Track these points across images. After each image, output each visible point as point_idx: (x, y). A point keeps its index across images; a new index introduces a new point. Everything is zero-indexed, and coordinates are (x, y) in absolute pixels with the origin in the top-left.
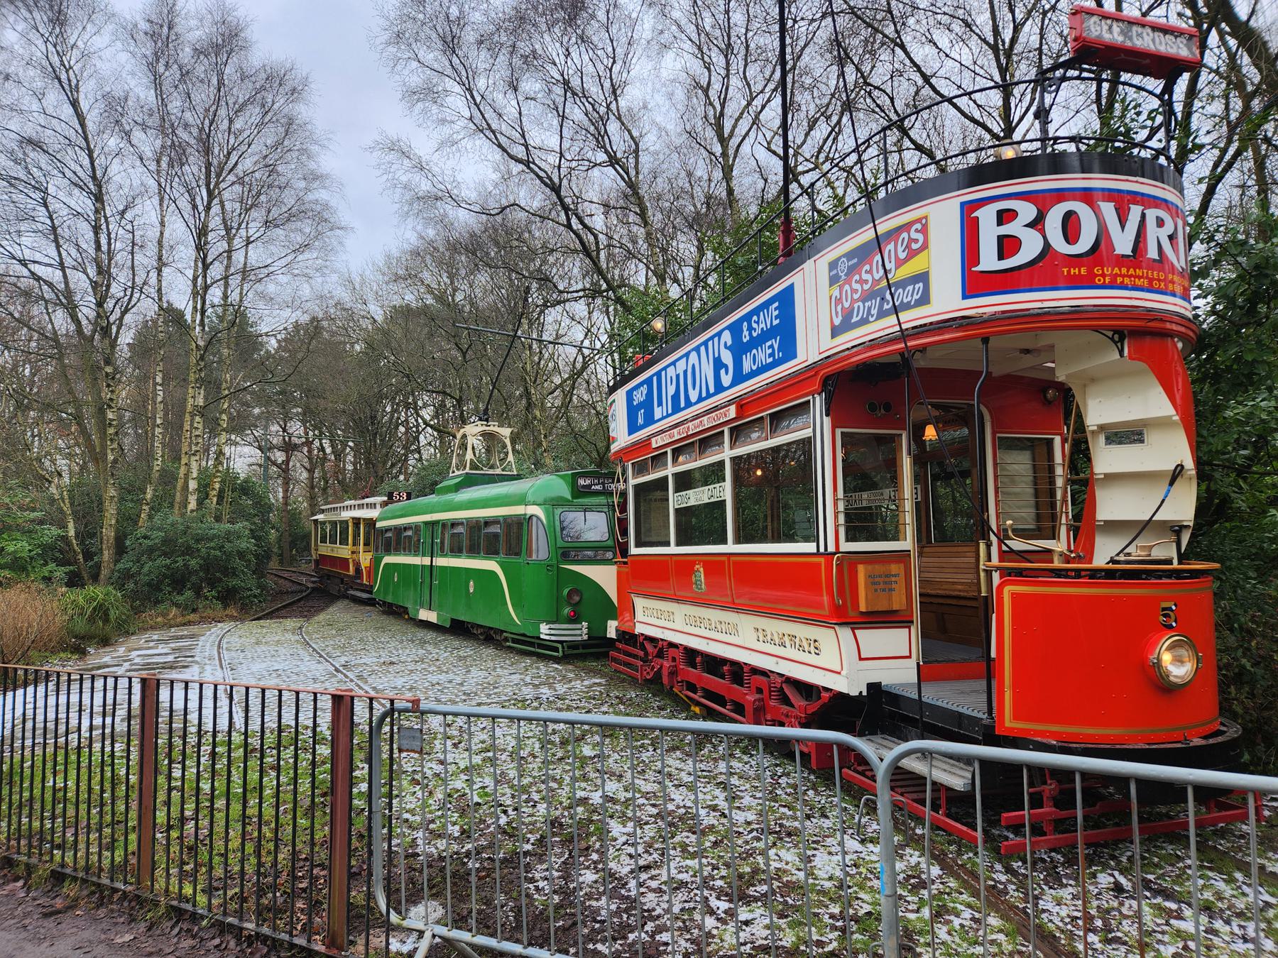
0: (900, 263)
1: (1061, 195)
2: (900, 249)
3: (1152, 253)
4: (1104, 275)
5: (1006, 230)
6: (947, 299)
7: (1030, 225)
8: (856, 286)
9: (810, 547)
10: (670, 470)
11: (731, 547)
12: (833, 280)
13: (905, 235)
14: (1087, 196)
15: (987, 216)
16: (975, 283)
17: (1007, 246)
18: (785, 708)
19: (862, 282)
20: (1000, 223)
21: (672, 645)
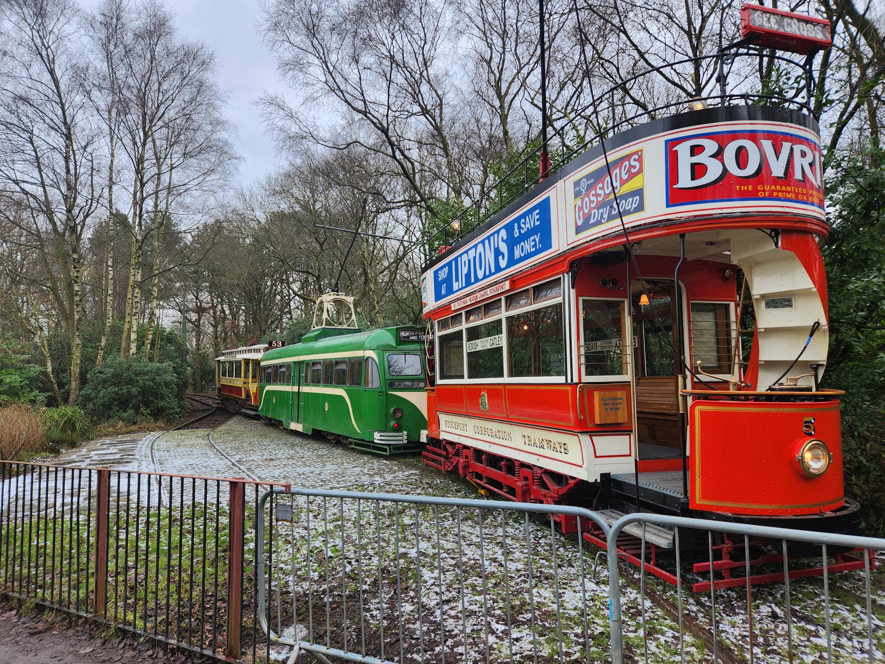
0: (623, 182)
1: (734, 135)
2: (623, 173)
3: (798, 175)
4: (764, 191)
5: (697, 159)
6: (656, 207)
7: (713, 156)
8: (593, 198)
9: (561, 379)
10: (464, 326)
11: (506, 379)
12: (577, 194)
13: (627, 163)
14: (753, 136)
15: (683, 150)
16: (675, 196)
17: (698, 170)
18: (544, 491)
19: (597, 195)
20: (692, 154)
21: (465, 447)
